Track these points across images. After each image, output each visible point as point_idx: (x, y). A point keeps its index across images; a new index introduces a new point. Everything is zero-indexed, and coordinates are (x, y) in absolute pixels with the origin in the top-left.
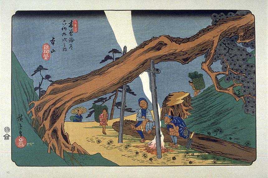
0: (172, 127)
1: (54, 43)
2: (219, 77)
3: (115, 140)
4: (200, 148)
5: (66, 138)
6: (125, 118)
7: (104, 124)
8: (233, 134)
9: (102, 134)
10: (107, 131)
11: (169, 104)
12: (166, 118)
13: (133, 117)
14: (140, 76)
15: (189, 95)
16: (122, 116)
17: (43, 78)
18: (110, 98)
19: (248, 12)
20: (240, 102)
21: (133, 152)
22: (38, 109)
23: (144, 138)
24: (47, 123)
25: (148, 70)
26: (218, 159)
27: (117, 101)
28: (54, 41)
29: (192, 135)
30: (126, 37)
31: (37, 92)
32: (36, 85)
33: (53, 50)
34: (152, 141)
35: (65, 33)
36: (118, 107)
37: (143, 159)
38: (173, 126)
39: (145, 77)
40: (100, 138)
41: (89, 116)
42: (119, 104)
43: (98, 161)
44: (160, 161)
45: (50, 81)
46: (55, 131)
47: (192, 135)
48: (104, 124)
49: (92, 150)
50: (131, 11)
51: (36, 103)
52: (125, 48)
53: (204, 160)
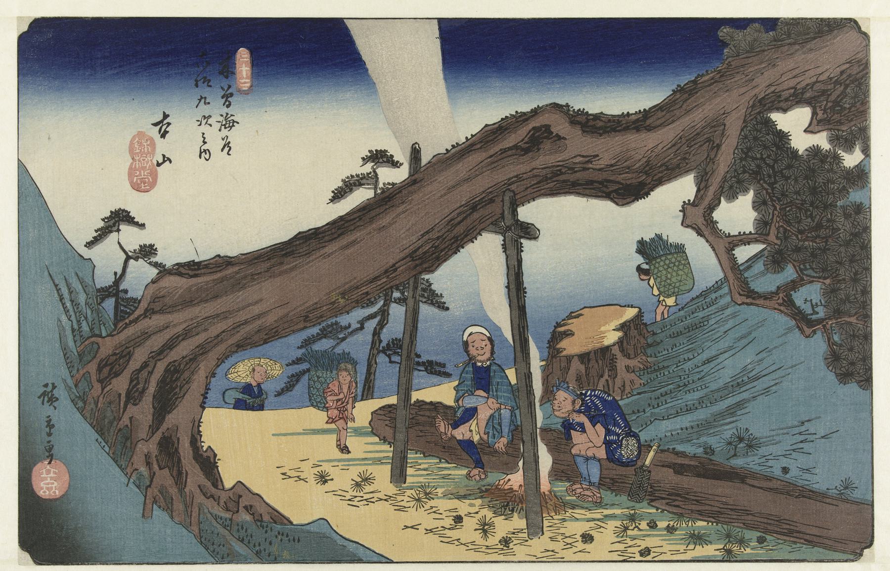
1: (166, 132)
2: (743, 254)
3: (382, 474)
4: (680, 503)
5: (208, 464)
6: (415, 396)
7: (341, 415)
8: (794, 455)
9: (338, 455)
10: (352, 442)
11: (570, 347)
12: (561, 395)
13: (442, 393)
15: (640, 315)
16: (405, 390)
17: (128, 257)
18: (362, 323)
19: (851, 24)
21: (445, 514)
24: (142, 412)
25: (495, 226)
26: (742, 542)
27: (386, 335)
28: (169, 124)
31: (109, 304)
32: (104, 278)
33: (164, 156)
34: (509, 477)
36: (390, 358)
37: (477, 537)
40: (326, 467)
41: (289, 387)
44: (539, 544)
46: (168, 446)
47: (652, 453)
48: (341, 415)
50: (436, 22)
53: (691, 547)
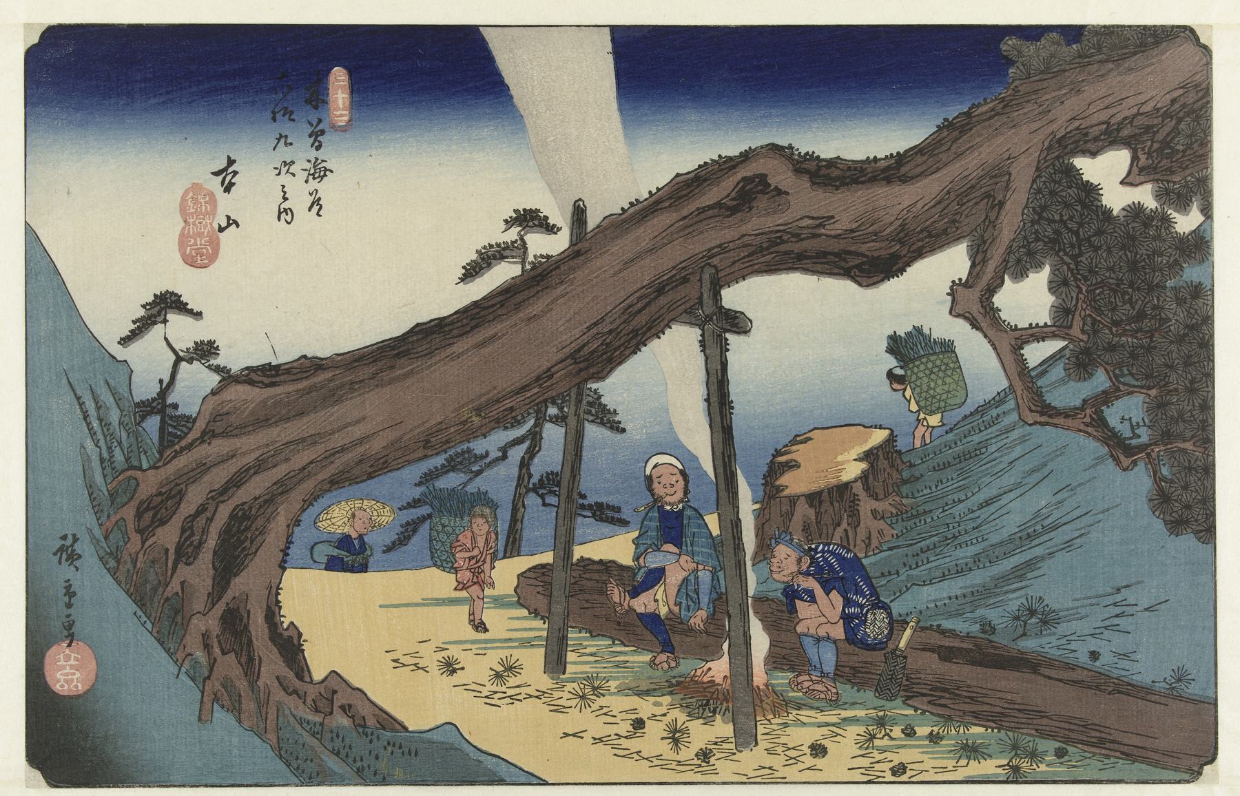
2: (1035, 354)
3: (533, 661)
4: (948, 702)
5: (290, 646)
6: (579, 552)
7: (476, 579)
9: (470, 634)
10: (491, 616)
11: (795, 484)
12: (782, 551)
13: (616, 547)
15: (892, 439)
16: (564, 544)
17: (179, 359)
18: (504, 451)
19: (1186, 33)
21: (620, 716)
26: (1034, 755)
27: (538, 468)
28: (235, 173)
31: (152, 424)
32: (145, 388)
33: (228, 218)
34: (709, 665)
35: (286, 137)
37: (665, 748)
40: (454, 652)
41: (403, 540)
44: (750, 759)
46: (234, 622)
47: (908, 632)
48: (476, 579)
50: (607, 30)
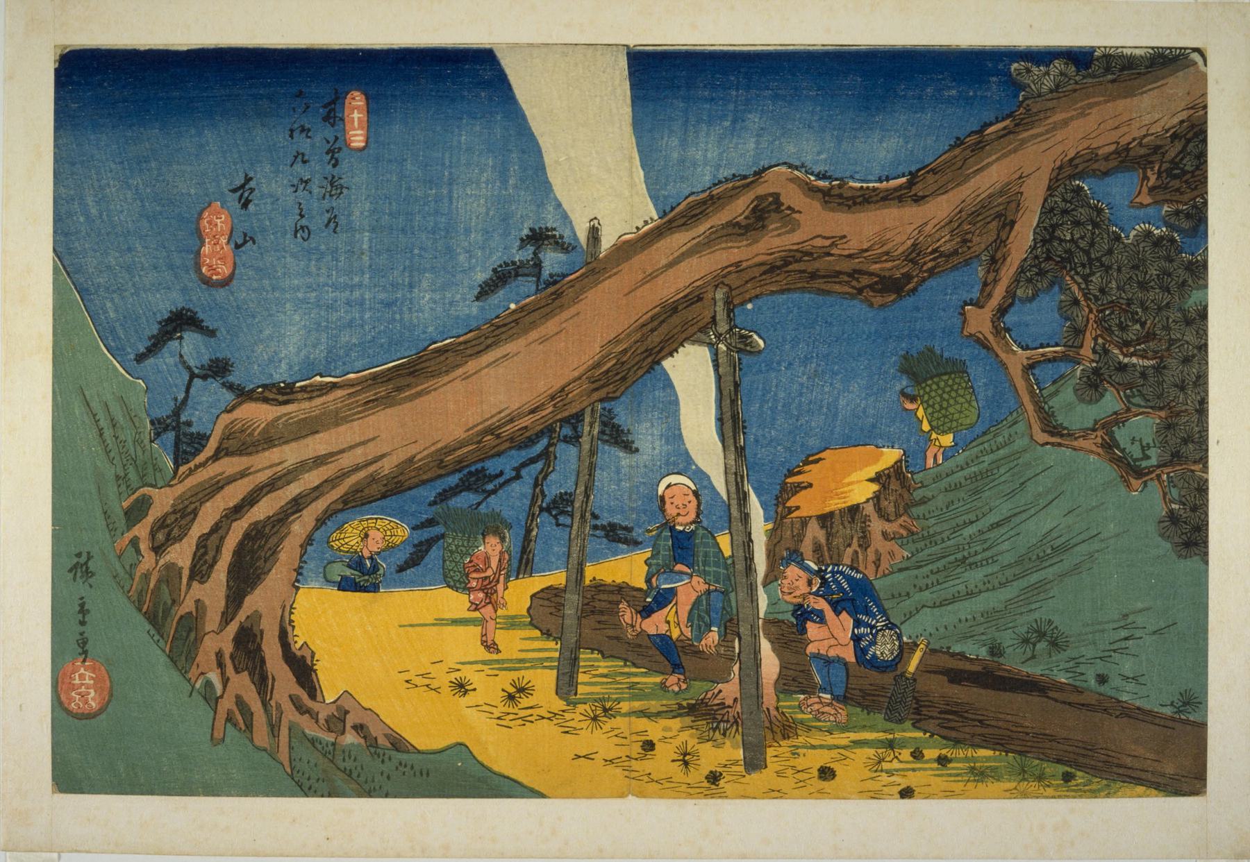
0: (820, 618)
3: (544, 681)
5: (303, 670)
6: (592, 572)
11: (806, 505)
14: (667, 364)
17: (193, 376)
20: (1151, 500)
22: (168, 531)
23: (683, 674)
27: (553, 488)
29: (918, 655)
30: (600, 179)
38: (822, 611)
39: (691, 372)
40: (468, 673)
42: (560, 506)
43: (457, 775)
45: (231, 387)
46: (248, 641)
47: (918, 655)
49: (425, 725)
51: (163, 501)
52: (594, 234)
